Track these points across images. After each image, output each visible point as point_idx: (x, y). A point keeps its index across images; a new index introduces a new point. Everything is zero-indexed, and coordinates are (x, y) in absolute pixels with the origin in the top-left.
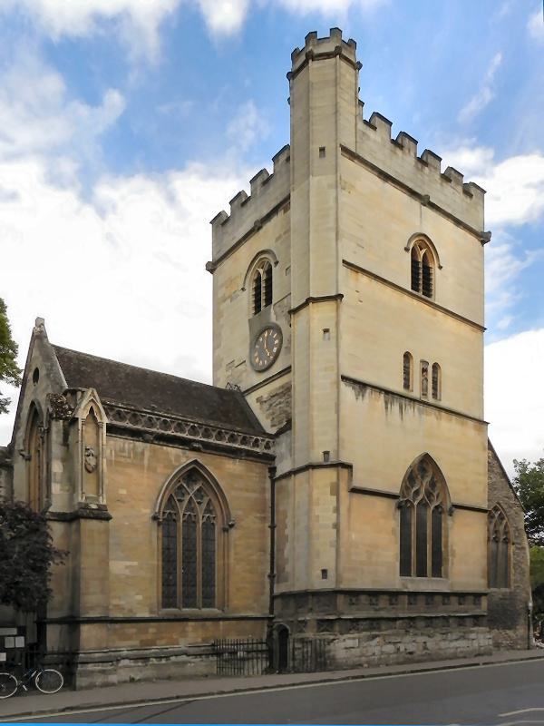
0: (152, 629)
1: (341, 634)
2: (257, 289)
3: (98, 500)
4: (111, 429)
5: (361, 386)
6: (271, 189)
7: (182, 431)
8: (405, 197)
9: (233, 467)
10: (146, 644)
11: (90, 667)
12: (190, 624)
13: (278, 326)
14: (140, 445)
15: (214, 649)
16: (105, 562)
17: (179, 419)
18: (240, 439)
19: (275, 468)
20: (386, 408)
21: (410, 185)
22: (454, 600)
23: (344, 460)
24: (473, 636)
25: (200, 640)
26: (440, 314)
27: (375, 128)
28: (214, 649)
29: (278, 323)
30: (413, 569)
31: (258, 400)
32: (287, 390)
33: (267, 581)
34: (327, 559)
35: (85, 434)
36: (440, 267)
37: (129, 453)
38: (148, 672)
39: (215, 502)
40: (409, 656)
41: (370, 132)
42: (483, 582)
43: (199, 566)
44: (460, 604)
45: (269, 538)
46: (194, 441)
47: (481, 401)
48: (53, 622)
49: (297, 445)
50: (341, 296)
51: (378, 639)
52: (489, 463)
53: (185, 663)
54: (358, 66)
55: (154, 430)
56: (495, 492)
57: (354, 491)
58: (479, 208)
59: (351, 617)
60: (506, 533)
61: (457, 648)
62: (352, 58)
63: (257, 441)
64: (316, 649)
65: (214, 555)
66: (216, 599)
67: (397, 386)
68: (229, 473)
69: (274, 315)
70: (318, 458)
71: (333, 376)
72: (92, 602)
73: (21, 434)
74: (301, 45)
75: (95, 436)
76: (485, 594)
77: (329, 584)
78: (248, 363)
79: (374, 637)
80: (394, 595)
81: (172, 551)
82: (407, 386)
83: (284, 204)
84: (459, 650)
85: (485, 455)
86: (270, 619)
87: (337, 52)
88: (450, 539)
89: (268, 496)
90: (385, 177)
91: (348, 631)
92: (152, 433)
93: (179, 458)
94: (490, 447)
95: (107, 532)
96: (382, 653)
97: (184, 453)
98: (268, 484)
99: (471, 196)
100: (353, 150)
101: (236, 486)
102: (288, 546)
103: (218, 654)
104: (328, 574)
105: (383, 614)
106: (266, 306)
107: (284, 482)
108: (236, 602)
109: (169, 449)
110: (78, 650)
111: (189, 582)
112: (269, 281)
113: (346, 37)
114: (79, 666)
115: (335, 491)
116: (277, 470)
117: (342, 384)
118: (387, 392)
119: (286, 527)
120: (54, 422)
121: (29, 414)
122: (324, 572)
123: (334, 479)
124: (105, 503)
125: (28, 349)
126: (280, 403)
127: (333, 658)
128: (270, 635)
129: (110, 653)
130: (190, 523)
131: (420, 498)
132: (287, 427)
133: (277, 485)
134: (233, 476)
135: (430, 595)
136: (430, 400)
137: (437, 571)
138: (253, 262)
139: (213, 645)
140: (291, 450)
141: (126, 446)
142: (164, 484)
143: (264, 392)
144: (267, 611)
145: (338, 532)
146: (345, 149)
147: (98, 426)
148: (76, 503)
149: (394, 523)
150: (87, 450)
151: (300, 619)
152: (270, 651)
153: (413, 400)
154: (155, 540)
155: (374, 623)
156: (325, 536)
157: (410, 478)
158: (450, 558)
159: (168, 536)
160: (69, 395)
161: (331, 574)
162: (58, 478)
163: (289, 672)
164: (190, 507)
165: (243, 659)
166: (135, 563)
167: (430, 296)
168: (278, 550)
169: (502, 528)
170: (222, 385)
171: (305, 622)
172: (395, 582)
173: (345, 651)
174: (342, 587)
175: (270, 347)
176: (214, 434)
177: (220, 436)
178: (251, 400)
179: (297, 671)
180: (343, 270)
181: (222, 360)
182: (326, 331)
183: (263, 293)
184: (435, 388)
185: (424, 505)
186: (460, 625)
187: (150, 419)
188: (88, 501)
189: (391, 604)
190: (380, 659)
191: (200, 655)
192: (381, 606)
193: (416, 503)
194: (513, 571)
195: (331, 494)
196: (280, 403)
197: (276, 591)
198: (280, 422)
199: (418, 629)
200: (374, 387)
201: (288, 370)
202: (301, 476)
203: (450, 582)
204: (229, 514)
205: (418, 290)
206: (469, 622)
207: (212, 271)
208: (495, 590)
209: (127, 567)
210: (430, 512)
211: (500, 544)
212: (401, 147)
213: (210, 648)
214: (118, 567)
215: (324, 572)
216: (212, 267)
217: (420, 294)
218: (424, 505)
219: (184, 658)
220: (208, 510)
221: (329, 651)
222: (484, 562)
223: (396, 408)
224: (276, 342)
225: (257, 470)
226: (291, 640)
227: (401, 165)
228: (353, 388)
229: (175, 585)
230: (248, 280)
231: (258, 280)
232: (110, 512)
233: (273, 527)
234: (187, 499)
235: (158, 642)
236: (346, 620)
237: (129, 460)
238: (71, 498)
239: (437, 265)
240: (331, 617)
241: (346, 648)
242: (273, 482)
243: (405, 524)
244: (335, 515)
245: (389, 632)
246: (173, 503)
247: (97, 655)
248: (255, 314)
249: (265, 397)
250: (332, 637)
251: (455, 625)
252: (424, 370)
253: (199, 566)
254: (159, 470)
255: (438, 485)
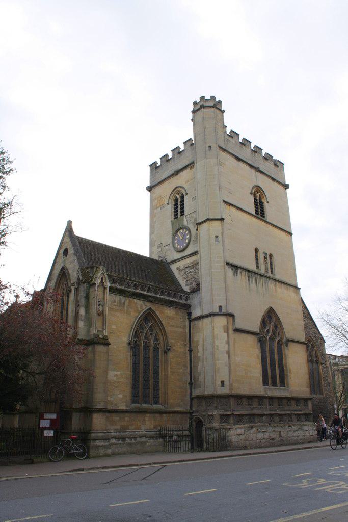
0: (127, 417)
1: (235, 425)
2: (176, 205)
3: (103, 333)
4: (112, 290)
5: (235, 268)
6: (182, 157)
7: (143, 290)
8: (248, 168)
9: (169, 312)
10: (124, 428)
11: (98, 443)
12: (148, 415)
13: (188, 228)
14: (122, 299)
15: (160, 434)
16: (106, 372)
17: (142, 283)
18: (172, 295)
19: (191, 313)
20: (249, 280)
21: (250, 162)
22: (293, 402)
23: (230, 311)
24: (306, 428)
25: (152, 427)
26: (270, 227)
27: (232, 137)
28: (160, 434)
29: (189, 226)
30: (270, 381)
31: (177, 268)
32: (195, 265)
33: (188, 386)
34: (223, 375)
35: (97, 292)
36: (268, 202)
37: (118, 303)
38: (125, 449)
39: (160, 334)
40: (271, 441)
41: (231, 139)
42: (308, 390)
43: (151, 376)
44: (297, 405)
45: (189, 358)
46: (149, 296)
47: (296, 280)
48: (77, 410)
49: (204, 300)
50: (224, 219)
51: (254, 429)
52: (303, 311)
53: (145, 443)
54: (223, 111)
55: (130, 289)
56: (308, 330)
57: (237, 330)
58: (282, 172)
59: (239, 413)
60: (317, 357)
61: (298, 437)
62: (220, 108)
63: (181, 296)
64: (221, 437)
65: (159, 369)
66: (160, 399)
67: (253, 267)
68: (166, 314)
69: (186, 221)
70: (216, 310)
71: (222, 263)
72: (99, 399)
73: (53, 284)
74: (198, 101)
75: (102, 293)
76: (310, 399)
77: (225, 391)
78: (171, 245)
79: (252, 427)
80: (261, 398)
81: (137, 365)
82: (257, 267)
83: (191, 165)
84: (299, 438)
85: (300, 309)
86: (191, 413)
87: (214, 106)
88: (288, 362)
89: (187, 330)
90: (238, 159)
91: (238, 423)
92: (129, 292)
93: (141, 306)
94: (303, 302)
95: (107, 352)
96: (257, 439)
97: (144, 304)
98: (187, 324)
99: (278, 166)
100: (224, 148)
101: (171, 323)
102: (200, 364)
103: (163, 437)
104: (225, 383)
105: (256, 412)
106: (181, 215)
107: (196, 322)
108: (171, 401)
109: (137, 301)
110: (89, 432)
111: (274, 377)
112: (182, 201)
113: (217, 100)
114: (92, 441)
115: (226, 330)
116: (192, 314)
117: (227, 267)
118: (249, 271)
119: (199, 352)
120: (82, 285)
121: (59, 274)
122: (223, 382)
123: (225, 323)
124: (106, 334)
125: (62, 235)
126: (191, 272)
127: (231, 442)
128: (191, 425)
129: (107, 434)
130: (146, 347)
131: (270, 334)
132: (197, 289)
133: (192, 324)
134: (169, 317)
135: (280, 399)
136: (270, 275)
137: (283, 384)
138: (174, 190)
139: (160, 431)
140: (200, 303)
141: (116, 299)
142: (135, 321)
143: (182, 264)
144: (188, 408)
145: (229, 357)
146: (220, 147)
147: (105, 288)
148: (92, 333)
149: (257, 351)
150: (99, 302)
151: (209, 414)
152: (191, 436)
153: (262, 275)
154: (129, 358)
155: (252, 417)
156: (222, 359)
157: (264, 323)
158: (289, 374)
159: (135, 355)
160: (89, 269)
161: (227, 383)
162: (83, 318)
163: (204, 451)
164: (146, 338)
165: (176, 442)
166: (119, 373)
167: (264, 217)
168: (194, 366)
169: (314, 353)
170: (156, 257)
171: (212, 416)
172: (259, 389)
173: (236, 436)
174: (233, 392)
175: (184, 238)
176: (160, 292)
177: (162, 294)
178: (174, 267)
179: (208, 450)
180: (223, 205)
181: (155, 241)
182: (217, 237)
183: (179, 208)
184: (271, 268)
185: (272, 339)
186: (298, 420)
187: (128, 283)
188: (99, 333)
189: (260, 405)
190: (256, 443)
191: (153, 437)
192: (254, 406)
193: (268, 338)
194: (323, 382)
195: (224, 332)
196: (191, 272)
197: (194, 394)
198: (191, 284)
199: (275, 423)
200: (242, 268)
201: (195, 253)
202: (207, 320)
203: (290, 390)
204: (167, 342)
205: (258, 214)
206: (303, 418)
207: (149, 191)
208: (315, 396)
209: (114, 376)
210: (275, 344)
211: (314, 364)
212: (244, 145)
213: (158, 433)
214: (112, 375)
215: (223, 382)
216: (150, 189)
217: (260, 216)
218: (272, 339)
219: (144, 439)
220: (156, 339)
221: (228, 437)
222: (307, 376)
223: (253, 285)
224: (188, 236)
225: (181, 314)
226: (204, 428)
227: (245, 154)
228: (232, 269)
229: (138, 388)
230: (170, 200)
231: (176, 200)
232: (110, 340)
233: (190, 351)
234: (145, 331)
235: (130, 427)
236: (236, 415)
237: (117, 308)
238: (88, 331)
239: (266, 200)
240: (228, 413)
241: (237, 435)
242: (190, 322)
243: (263, 352)
244: (227, 345)
245: (260, 424)
246: (138, 333)
247: (100, 434)
248: (175, 218)
249: (182, 267)
250: (229, 427)
251: (295, 420)
252: (266, 258)
253: (151, 376)
254: (132, 314)
255: (279, 326)
